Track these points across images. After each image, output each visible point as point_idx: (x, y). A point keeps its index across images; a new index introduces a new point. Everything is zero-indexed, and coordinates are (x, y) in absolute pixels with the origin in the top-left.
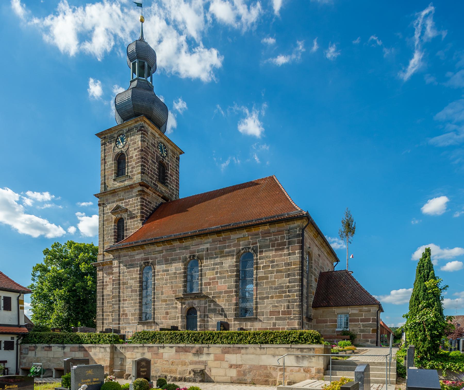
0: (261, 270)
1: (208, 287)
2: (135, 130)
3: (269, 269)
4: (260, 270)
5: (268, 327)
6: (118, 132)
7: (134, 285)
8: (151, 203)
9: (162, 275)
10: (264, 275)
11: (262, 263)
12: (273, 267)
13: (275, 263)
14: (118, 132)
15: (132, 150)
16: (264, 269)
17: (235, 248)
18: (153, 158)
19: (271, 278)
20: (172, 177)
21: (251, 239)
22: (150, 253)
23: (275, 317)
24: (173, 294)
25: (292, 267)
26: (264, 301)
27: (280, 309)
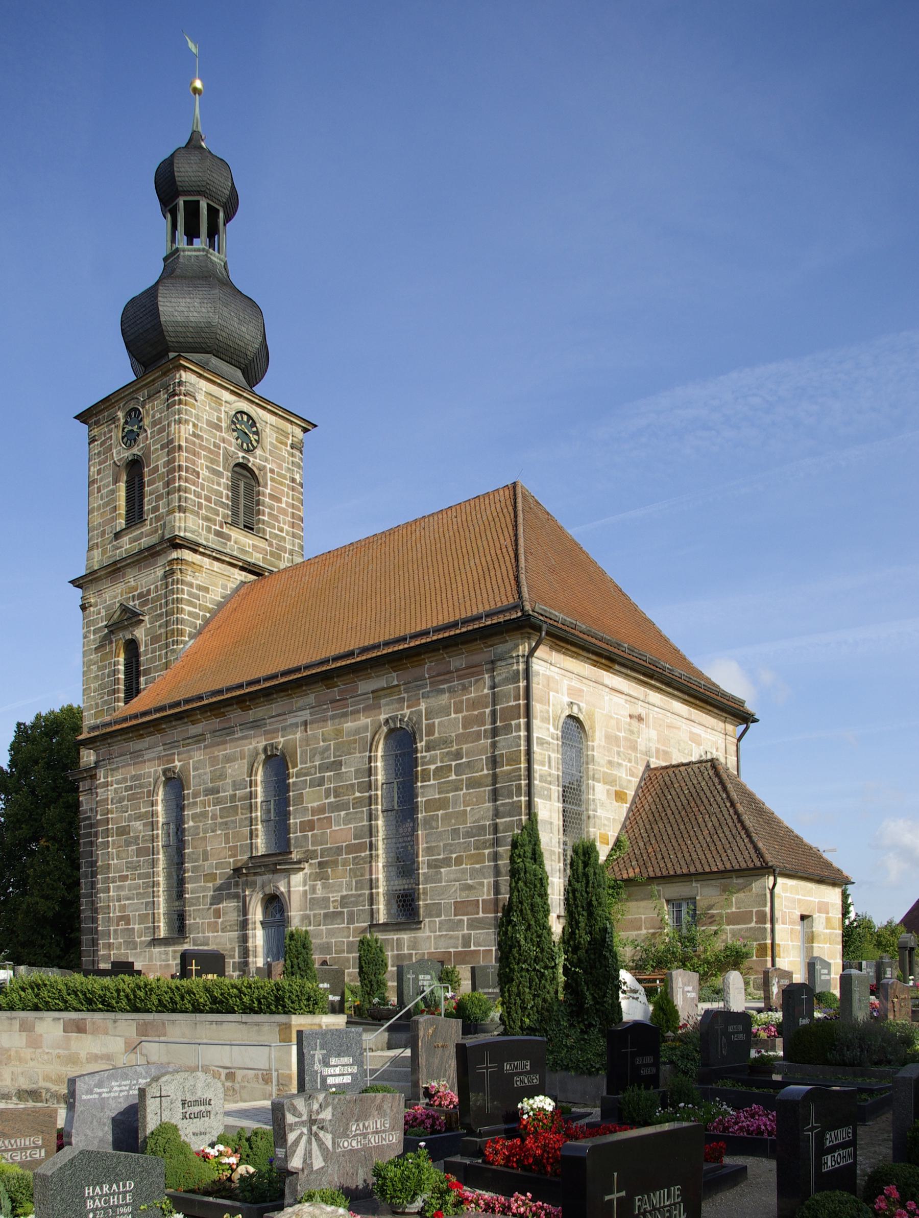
0: (432, 782)
1: (310, 834)
2: (164, 394)
3: (450, 778)
4: (429, 780)
5: (452, 950)
6: (126, 403)
7: (142, 834)
8: (206, 590)
9: (203, 804)
10: (437, 796)
11: (433, 761)
12: (459, 770)
13: (464, 760)
14: (126, 403)
15: (156, 449)
16: (438, 777)
17: (369, 720)
18: (212, 461)
19: (455, 803)
20: (280, 501)
21: (405, 693)
22: (176, 741)
23: (468, 919)
24: (230, 857)
25: (505, 768)
26: (441, 873)
27: (480, 896)
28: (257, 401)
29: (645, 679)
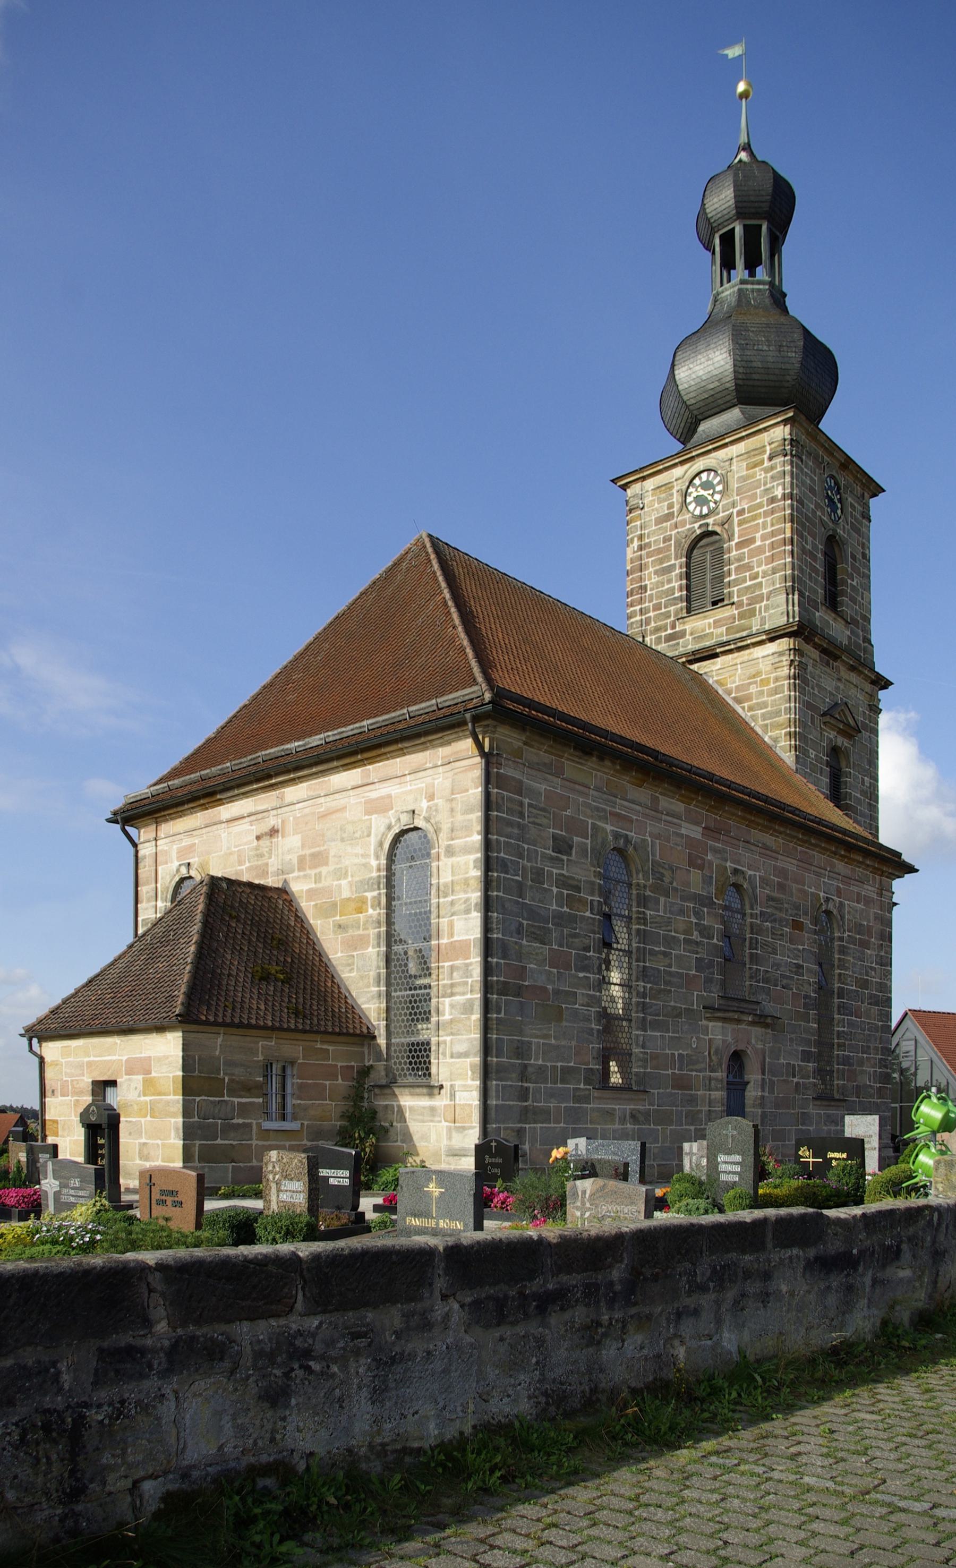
28: (710, 447)
29: (267, 783)
